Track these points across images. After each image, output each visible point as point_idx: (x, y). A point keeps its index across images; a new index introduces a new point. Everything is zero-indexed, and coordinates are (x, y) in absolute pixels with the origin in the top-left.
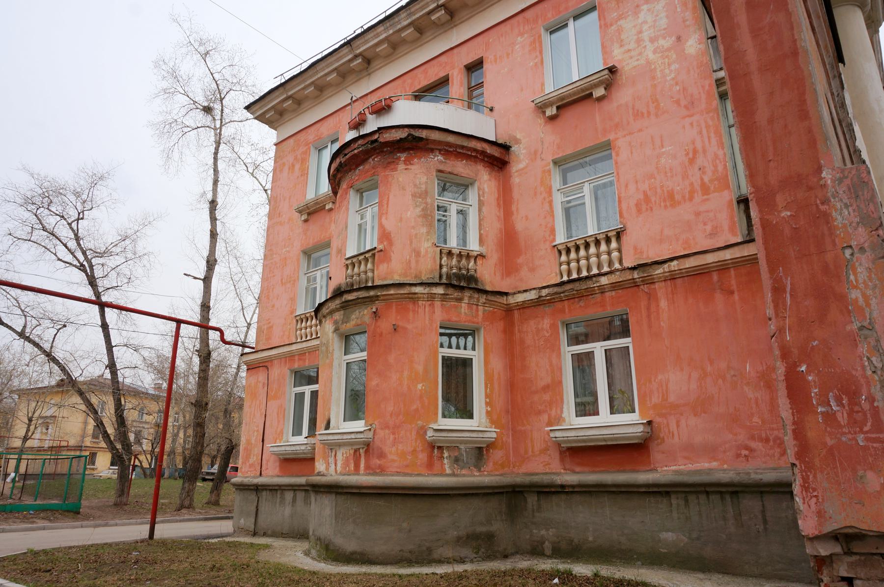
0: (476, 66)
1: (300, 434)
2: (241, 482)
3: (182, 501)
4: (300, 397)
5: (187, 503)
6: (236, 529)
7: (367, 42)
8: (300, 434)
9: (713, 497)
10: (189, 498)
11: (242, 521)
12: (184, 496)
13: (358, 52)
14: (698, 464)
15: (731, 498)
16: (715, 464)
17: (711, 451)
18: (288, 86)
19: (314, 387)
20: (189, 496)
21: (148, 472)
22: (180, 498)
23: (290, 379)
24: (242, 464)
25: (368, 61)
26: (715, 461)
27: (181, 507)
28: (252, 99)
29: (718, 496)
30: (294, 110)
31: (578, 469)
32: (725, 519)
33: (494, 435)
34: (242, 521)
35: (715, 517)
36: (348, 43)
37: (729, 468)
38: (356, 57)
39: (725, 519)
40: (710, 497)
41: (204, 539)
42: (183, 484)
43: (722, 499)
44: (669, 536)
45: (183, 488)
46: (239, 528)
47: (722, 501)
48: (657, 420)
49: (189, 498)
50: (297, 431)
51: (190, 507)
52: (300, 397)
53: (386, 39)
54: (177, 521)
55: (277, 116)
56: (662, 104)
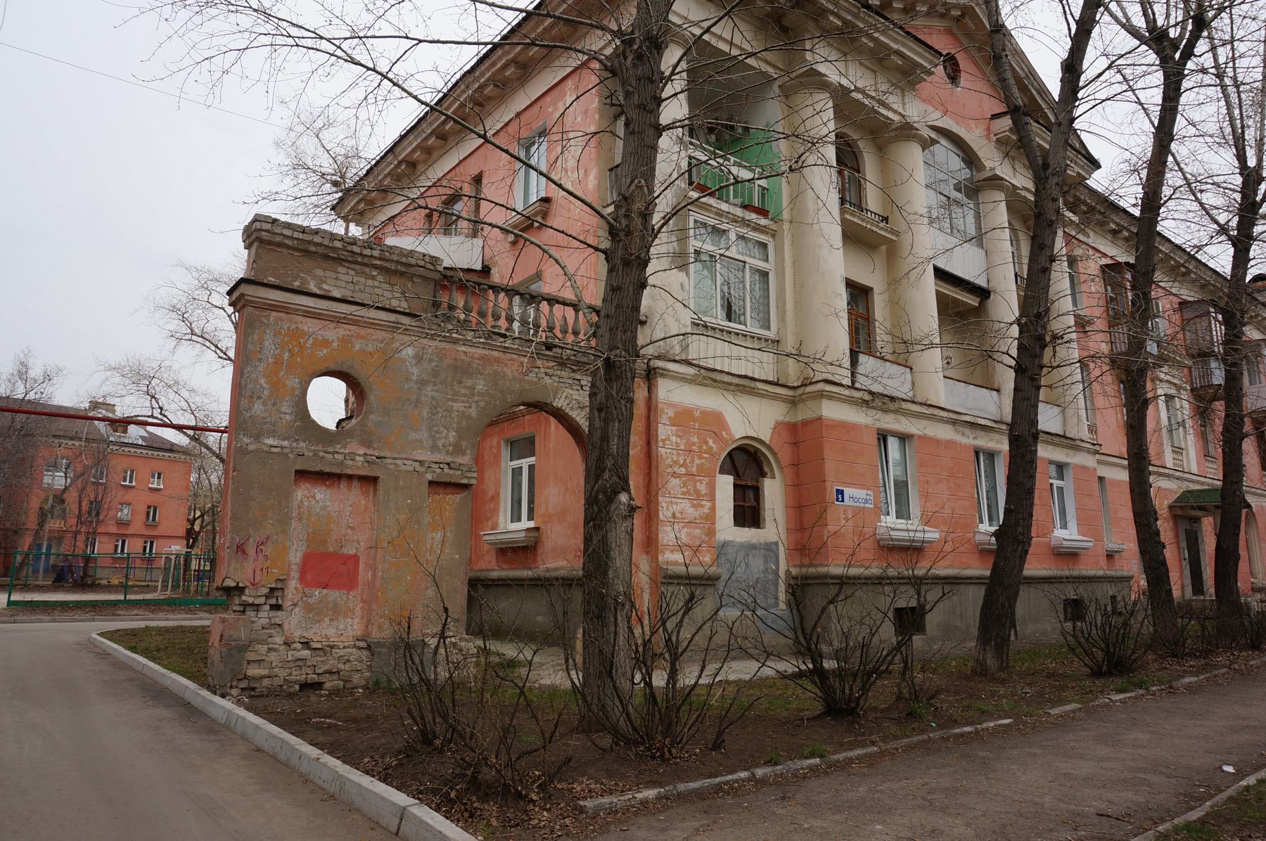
0: (478, 180)
1: (519, 520)
4: (517, 472)
7: (404, 149)
8: (519, 520)
13: (400, 158)
18: (398, 149)
19: (532, 460)
23: (505, 452)
25: (412, 165)
28: (229, 288)
30: (425, 161)
31: (504, 566)
33: (1091, 544)
36: (391, 150)
38: (400, 163)
44: (540, 619)
48: (542, 527)
50: (516, 517)
52: (517, 472)
53: (418, 146)
55: (425, 156)
56: (57, 480)
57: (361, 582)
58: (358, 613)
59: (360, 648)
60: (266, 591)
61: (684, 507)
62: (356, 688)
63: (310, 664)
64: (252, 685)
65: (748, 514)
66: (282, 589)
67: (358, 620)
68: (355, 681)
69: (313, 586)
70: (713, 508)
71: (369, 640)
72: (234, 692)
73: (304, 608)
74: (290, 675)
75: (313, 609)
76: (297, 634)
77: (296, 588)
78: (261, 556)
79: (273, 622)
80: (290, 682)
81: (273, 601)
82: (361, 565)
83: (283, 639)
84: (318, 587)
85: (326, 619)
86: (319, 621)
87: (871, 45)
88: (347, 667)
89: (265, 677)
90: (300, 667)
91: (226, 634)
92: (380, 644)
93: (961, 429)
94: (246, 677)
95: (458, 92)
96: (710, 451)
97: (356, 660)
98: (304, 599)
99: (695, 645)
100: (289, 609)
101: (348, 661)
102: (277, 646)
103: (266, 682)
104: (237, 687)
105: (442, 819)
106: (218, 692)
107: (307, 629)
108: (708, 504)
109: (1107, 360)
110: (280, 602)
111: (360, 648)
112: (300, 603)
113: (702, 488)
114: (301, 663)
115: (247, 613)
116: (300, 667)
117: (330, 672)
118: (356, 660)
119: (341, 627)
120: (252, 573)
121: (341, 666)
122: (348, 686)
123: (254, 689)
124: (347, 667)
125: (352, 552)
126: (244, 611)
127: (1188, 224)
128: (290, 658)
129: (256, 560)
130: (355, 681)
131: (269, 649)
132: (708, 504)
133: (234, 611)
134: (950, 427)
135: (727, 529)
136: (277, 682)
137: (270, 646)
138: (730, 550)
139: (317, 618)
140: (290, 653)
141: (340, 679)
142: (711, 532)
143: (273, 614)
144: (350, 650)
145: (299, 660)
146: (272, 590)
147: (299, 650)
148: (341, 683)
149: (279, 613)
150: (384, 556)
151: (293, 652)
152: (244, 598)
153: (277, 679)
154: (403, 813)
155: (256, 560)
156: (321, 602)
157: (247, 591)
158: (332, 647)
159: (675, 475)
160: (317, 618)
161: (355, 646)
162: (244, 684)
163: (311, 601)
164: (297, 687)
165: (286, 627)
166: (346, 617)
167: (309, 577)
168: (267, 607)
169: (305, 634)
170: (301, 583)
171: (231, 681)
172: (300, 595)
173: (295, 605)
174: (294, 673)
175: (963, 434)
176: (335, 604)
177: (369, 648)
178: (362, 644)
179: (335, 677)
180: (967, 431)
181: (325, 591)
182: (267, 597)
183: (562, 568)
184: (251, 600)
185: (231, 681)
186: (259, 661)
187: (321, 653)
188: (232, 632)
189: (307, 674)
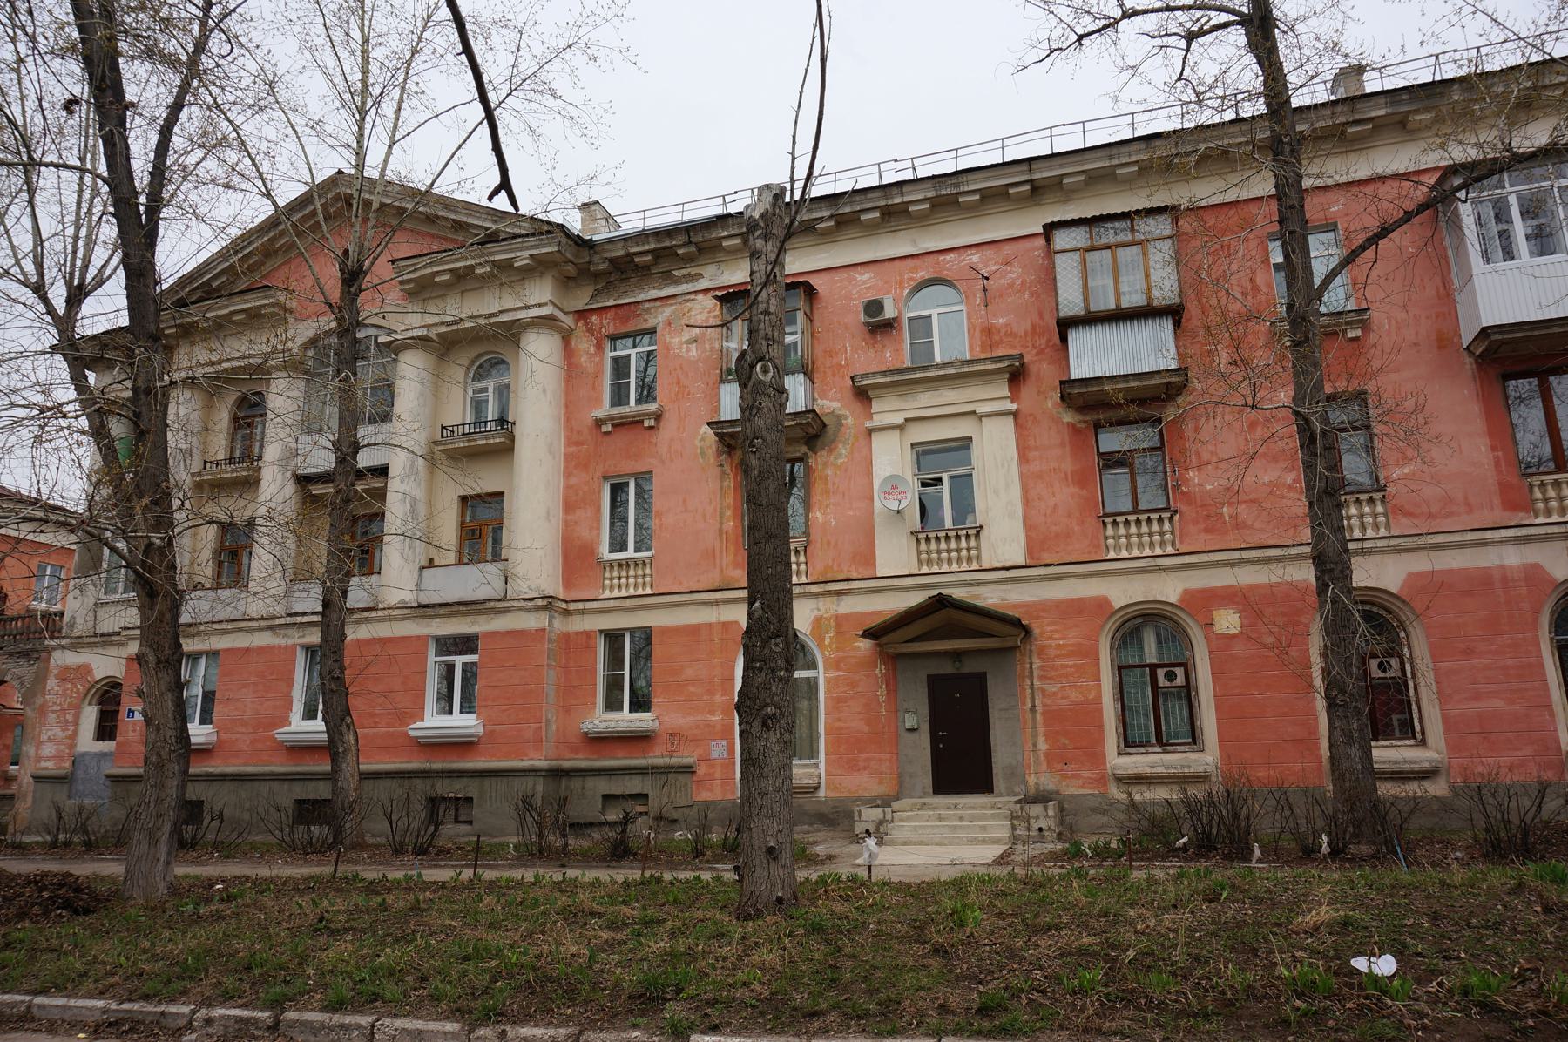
61: (57, 732)
65: (105, 731)
70: (75, 733)
87: (649, 257)
93: (282, 632)
95: (1214, 133)
96: (78, 692)
99: (1175, 656)
105: (21, 872)
108: (71, 728)
109: (306, 440)
113: (70, 717)
127: (290, 131)
132: (71, 728)
134: (268, 633)
135: (87, 742)
138: (87, 758)
142: (72, 746)
159: (53, 712)
175: (285, 636)
180: (290, 631)
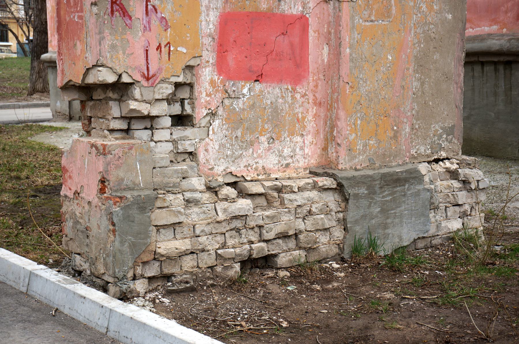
2: (50, 59)
3: (34, 83)
5: (39, 86)
6: (54, 113)
9: (488, 68)
10: (41, 80)
11: (58, 104)
12: (34, 77)
14: (479, 29)
15: (505, 69)
16: (495, 28)
17: (143, 7)
20: (40, 77)
21: (27, 48)
22: (31, 80)
24: (51, 37)
26: (495, 24)
27: (33, 92)
29: (492, 68)
32: (496, 94)
34: (58, 104)
35: (487, 92)
37: (508, 32)
39: (496, 94)
40: (485, 68)
41: (16, 124)
42: (32, 63)
43: (496, 70)
45: (33, 68)
46: (56, 112)
47: (496, 73)
49: (41, 80)
51: (45, 90)
54: (24, 107)
57: (312, 66)
58: (310, 126)
59: (325, 189)
60: (168, 90)
62: (325, 260)
63: (253, 224)
64: (166, 271)
66: (191, 86)
67: (309, 138)
68: (323, 249)
69: (240, 79)
71: (340, 175)
72: (140, 286)
73: (228, 120)
74: (224, 246)
75: (241, 121)
76: (219, 169)
77: (212, 83)
78: (155, 22)
79: (181, 149)
80: (225, 259)
81: (176, 109)
82: (312, 34)
83: (203, 180)
84: (247, 79)
85: (263, 139)
86: (251, 143)
88: (309, 224)
89: (186, 253)
90: (238, 230)
91: (112, 178)
92: (356, 181)
94: (157, 257)
97: (321, 212)
98: (227, 102)
100: (204, 122)
101: (310, 213)
102: (197, 195)
103: (188, 263)
104: (142, 276)
106: (112, 288)
107: (235, 159)
110: (188, 109)
111: (325, 189)
112: (220, 112)
114: (238, 224)
115: (138, 134)
116: (238, 230)
117: (284, 236)
118: (321, 212)
119: (287, 152)
120: (143, 56)
121: (300, 225)
122: (314, 257)
123: (168, 277)
124: (309, 224)
125: (296, 10)
126: (127, 131)
128: (221, 216)
129: (147, 28)
130: (323, 249)
131: (188, 201)
133: (112, 131)
136: (207, 260)
137: (188, 195)
139: (248, 137)
140: (221, 206)
141: (300, 248)
143: (179, 132)
144: (307, 194)
145: (236, 217)
146: (178, 85)
147: (233, 201)
148: (303, 253)
149: (188, 132)
150: (352, 18)
151: (225, 204)
152: (133, 105)
153: (204, 255)
154: (31, 274)
155: (147, 28)
156: (253, 106)
157: (137, 92)
158: (279, 190)
160: (248, 137)
161: (315, 186)
162: (153, 271)
163: (239, 105)
164: (237, 267)
165: (201, 156)
166: (292, 134)
167: (231, 60)
168: (167, 122)
169: (233, 169)
170: (219, 74)
171: (134, 267)
172: (219, 95)
173: (213, 114)
174: (230, 242)
176: (275, 110)
177: (340, 188)
178: (324, 181)
179: (292, 243)
181: (258, 86)
182: (170, 100)
183: (490, 35)
184: (145, 109)
185: (134, 267)
186: (174, 226)
187: (262, 201)
188: (121, 174)
189: (252, 242)
